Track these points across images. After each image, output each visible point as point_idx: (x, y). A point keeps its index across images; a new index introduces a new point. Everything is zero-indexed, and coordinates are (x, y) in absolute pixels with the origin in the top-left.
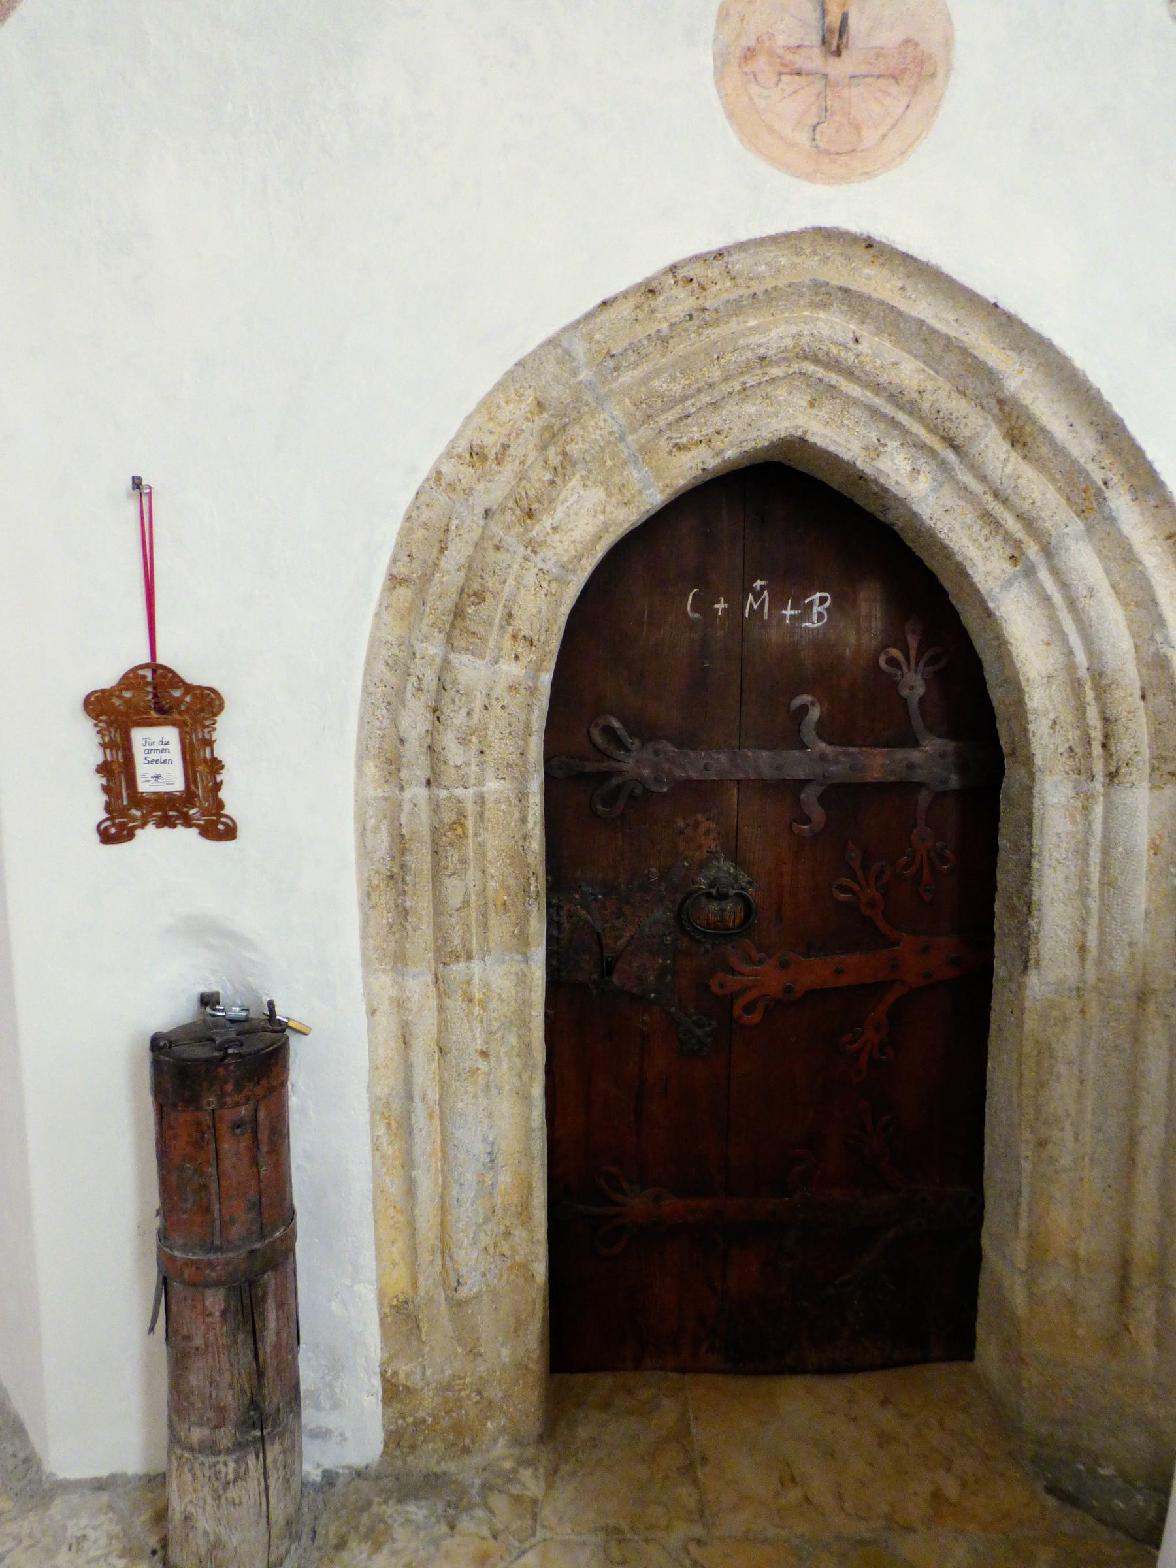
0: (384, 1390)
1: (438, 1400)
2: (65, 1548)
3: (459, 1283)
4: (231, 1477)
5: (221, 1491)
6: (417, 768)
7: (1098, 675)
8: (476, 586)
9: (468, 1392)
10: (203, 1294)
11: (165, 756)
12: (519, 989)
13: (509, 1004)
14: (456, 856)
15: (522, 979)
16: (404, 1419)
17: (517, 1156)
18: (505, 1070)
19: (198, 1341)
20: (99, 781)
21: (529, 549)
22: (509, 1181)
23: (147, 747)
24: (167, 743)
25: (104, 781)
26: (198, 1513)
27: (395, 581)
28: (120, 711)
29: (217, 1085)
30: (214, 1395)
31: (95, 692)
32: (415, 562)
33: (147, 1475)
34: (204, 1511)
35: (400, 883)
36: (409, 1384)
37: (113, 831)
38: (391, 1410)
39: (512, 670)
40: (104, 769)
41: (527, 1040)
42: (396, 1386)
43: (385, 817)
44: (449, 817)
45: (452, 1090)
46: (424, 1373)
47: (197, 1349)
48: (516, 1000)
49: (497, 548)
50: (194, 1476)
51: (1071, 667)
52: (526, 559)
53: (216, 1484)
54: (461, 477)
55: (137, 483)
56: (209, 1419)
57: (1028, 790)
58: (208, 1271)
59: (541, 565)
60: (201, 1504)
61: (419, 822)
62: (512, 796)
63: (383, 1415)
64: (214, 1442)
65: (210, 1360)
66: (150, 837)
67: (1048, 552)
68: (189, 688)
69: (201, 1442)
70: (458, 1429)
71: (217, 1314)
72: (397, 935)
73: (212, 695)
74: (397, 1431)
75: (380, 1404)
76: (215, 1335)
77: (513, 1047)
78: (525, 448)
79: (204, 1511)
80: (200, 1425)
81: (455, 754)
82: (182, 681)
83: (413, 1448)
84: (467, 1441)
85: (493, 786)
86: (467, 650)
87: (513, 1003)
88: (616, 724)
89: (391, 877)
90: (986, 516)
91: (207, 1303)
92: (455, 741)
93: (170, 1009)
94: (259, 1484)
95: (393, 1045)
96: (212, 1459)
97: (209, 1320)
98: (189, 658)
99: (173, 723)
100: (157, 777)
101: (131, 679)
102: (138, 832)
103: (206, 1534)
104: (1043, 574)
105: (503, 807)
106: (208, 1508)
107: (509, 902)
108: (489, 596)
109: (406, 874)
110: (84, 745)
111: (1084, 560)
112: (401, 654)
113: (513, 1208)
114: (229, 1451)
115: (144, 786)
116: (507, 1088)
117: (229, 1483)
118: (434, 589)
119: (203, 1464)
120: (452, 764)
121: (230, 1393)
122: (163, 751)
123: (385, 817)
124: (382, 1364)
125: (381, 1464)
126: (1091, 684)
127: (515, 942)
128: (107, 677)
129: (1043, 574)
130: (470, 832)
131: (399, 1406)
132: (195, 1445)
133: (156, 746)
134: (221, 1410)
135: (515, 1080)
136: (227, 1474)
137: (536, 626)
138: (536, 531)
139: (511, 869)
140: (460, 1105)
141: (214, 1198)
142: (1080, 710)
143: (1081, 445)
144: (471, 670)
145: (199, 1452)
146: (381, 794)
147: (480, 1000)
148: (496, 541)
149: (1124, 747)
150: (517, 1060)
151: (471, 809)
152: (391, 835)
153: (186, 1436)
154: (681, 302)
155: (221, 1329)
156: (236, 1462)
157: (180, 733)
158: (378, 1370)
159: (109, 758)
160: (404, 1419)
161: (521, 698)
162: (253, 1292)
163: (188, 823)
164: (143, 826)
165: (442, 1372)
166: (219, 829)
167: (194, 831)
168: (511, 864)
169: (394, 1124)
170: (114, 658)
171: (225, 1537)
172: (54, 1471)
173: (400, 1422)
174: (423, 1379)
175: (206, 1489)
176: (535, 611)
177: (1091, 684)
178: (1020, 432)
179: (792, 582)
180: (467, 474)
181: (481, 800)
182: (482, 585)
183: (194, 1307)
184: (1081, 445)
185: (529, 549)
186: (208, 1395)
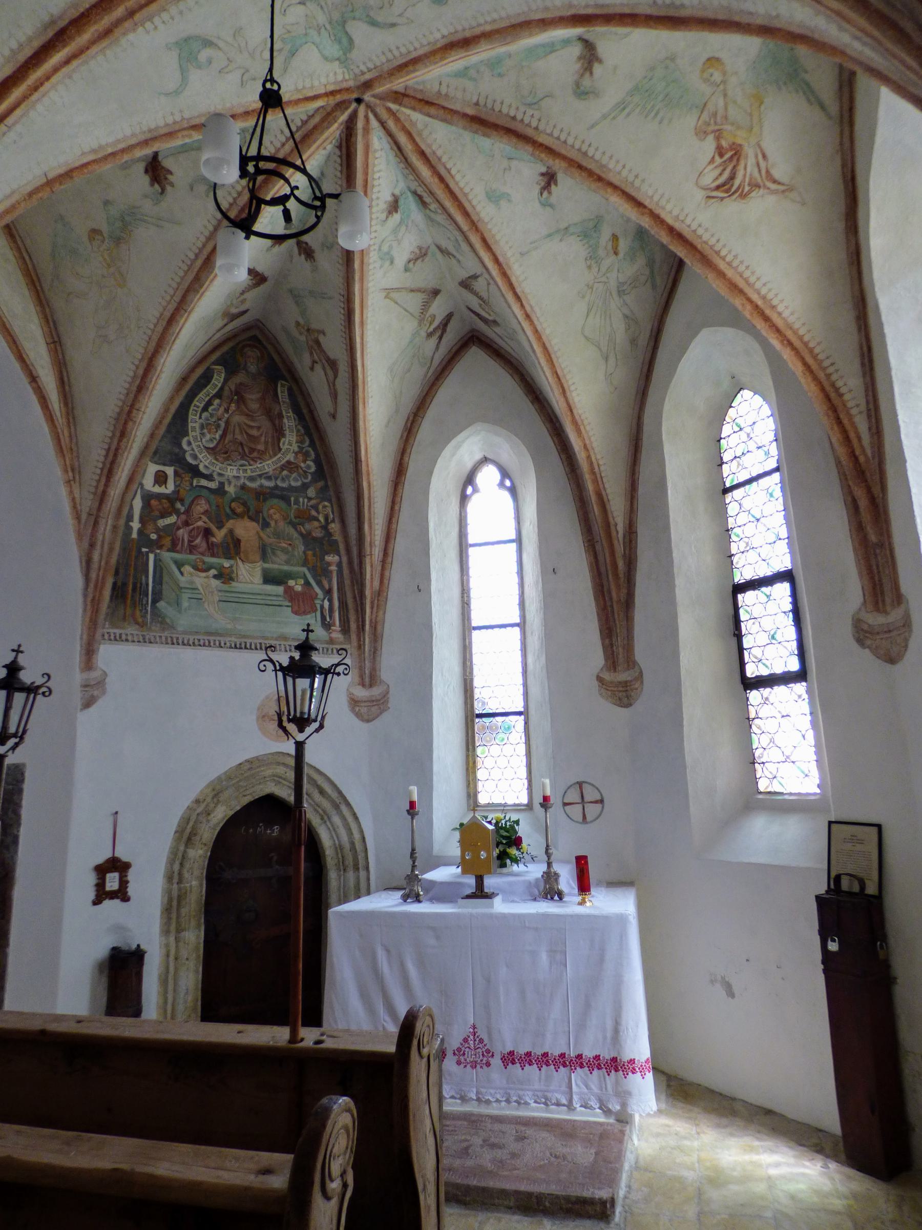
6: (175, 880)
7: (340, 846)
15: (198, 937)
18: (192, 964)
27: (176, 832)
28: (101, 871)
39: (201, 852)
44: (183, 891)
51: (335, 844)
57: (327, 875)
61: (175, 893)
67: (329, 818)
78: (209, 799)
81: (186, 875)
85: (194, 883)
88: (222, 864)
90: (315, 810)
98: (123, 854)
104: (328, 823)
109: (172, 908)
111: (336, 820)
118: (186, 835)
126: (339, 848)
129: (328, 823)
138: (209, 818)
142: (337, 854)
143: (334, 795)
144: (192, 853)
149: (347, 863)
151: (188, 889)
154: (248, 766)
170: (103, 855)
177: (339, 848)
178: (322, 792)
179: (269, 824)
181: (191, 886)
184: (334, 795)
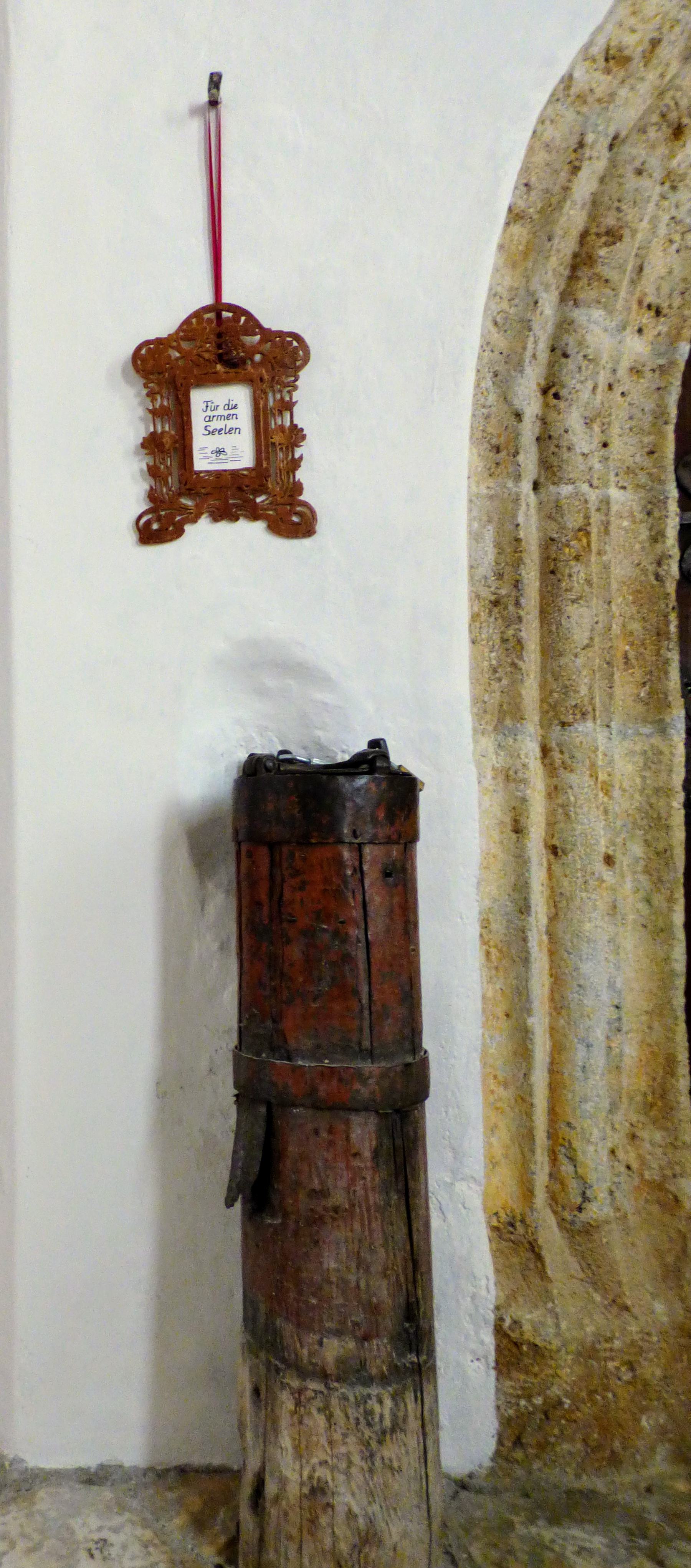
0: (499, 1349)
1: (579, 1370)
2: (83, 1555)
3: (585, 1198)
4: (387, 1423)
5: (374, 1444)
8: (610, 221)
9: (616, 1364)
10: (347, 1122)
11: (231, 423)
12: (647, 774)
13: (632, 797)
14: (582, 575)
15: (653, 760)
16: (529, 1398)
17: (644, 1018)
19: (338, 1198)
20: (140, 463)
21: (667, 185)
22: (634, 1054)
23: (209, 413)
24: (235, 407)
25: (150, 460)
26: (338, 1483)
28: (171, 370)
29: (303, 853)
30: (363, 1285)
31: (148, 342)
32: (533, 193)
33: (151, 1469)
34: (347, 1474)
35: (511, 608)
36: (537, 1341)
37: (155, 526)
38: (509, 1383)
40: (152, 444)
41: (661, 846)
42: (517, 1345)
43: (489, 521)
45: (578, 902)
46: (557, 1326)
47: (336, 1209)
48: (642, 791)
49: (639, 172)
50: (330, 1418)
52: (664, 197)
53: (367, 1433)
54: (594, 85)
55: (215, 81)
56: (356, 1324)
58: (357, 1086)
59: (674, 212)
60: (343, 1465)
62: (637, 508)
63: (498, 1390)
64: (363, 1365)
65: (357, 1226)
66: (204, 535)
68: (268, 335)
69: (340, 1361)
70: (605, 1424)
71: (367, 1154)
72: (505, 682)
73: (295, 344)
74: (520, 1415)
75: (493, 1373)
76: (365, 1188)
77: (637, 860)
79: (347, 1474)
80: (339, 1333)
82: (260, 326)
83: (542, 1446)
84: (617, 1444)
86: (599, 302)
87: (637, 796)
89: (496, 603)
91: (353, 1136)
92: (582, 421)
93: (204, 774)
94: (419, 1443)
95: (496, 835)
96: (360, 1390)
97: (356, 1163)
99: (249, 380)
100: (219, 452)
101: (189, 328)
102: (188, 528)
103: (351, 1515)
105: (625, 523)
106: (354, 1471)
107: (632, 655)
108: (626, 232)
109: (523, 591)
110: (123, 417)
112: (512, 311)
113: (639, 1098)
114: (384, 1380)
115: (202, 463)
116: (631, 917)
117: (384, 1432)
119: (345, 1398)
120: (578, 451)
121: (384, 1283)
122: (228, 417)
123: (489, 521)
124: (497, 1308)
125: (492, 1472)
127: (640, 708)
128: (163, 323)
130: (594, 546)
131: (522, 1377)
132: (331, 1368)
133: (221, 411)
134: (374, 1310)
135: (641, 906)
136: (382, 1417)
137: (665, 290)
139: (634, 609)
140: (588, 926)
141: (363, 974)
145: (338, 1380)
146: (485, 491)
147: (604, 782)
148: (637, 163)
150: (642, 878)
152: (498, 545)
153: (311, 1354)
155: (373, 1179)
156: (394, 1397)
157: (254, 392)
158: (491, 1317)
159: (159, 430)
160: (529, 1398)
161: (647, 382)
162: (405, 1130)
163: (254, 514)
164: (194, 521)
165: (581, 1327)
166: (292, 518)
167: (259, 526)
168: (634, 603)
169: (493, 951)
170: (168, 304)
171: (381, 1525)
172: (21, 1455)
173: (523, 1402)
174: (558, 1335)
175: (352, 1439)
176: (663, 271)
180: (602, 83)
181: (606, 502)
182: (619, 219)
183: (331, 1143)
185: (667, 185)
186: (353, 1284)
